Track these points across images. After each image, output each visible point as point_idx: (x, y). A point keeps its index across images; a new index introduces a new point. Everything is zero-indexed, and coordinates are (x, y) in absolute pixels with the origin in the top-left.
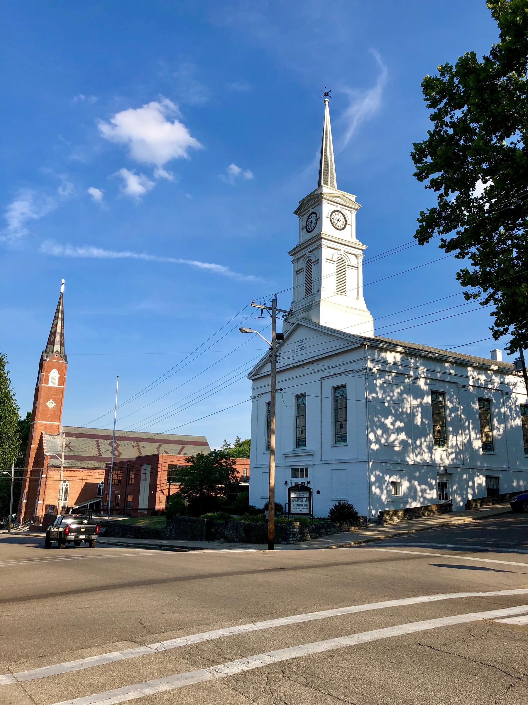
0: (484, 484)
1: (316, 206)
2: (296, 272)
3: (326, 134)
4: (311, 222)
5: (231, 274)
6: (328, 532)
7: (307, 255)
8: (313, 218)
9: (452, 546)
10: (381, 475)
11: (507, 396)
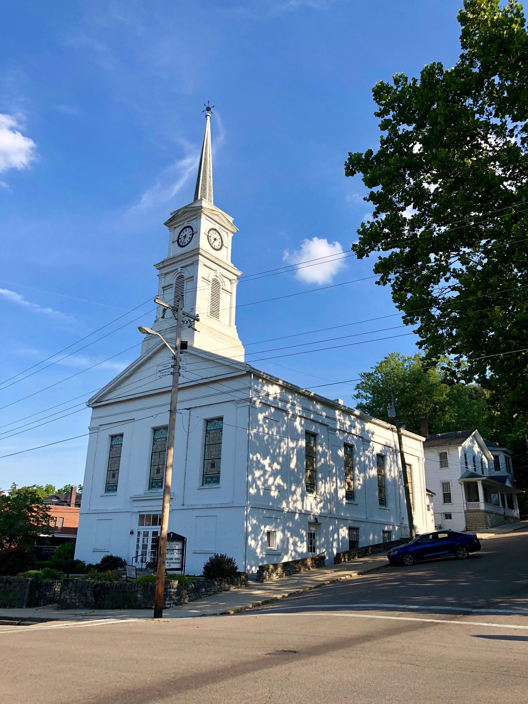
0: (347, 537)
1: (194, 219)
2: (163, 288)
3: (206, 148)
4: (185, 236)
5: (26, 303)
6: (207, 592)
7: (179, 270)
8: (188, 232)
9: (416, 607)
10: (257, 523)
11: (367, 443)
